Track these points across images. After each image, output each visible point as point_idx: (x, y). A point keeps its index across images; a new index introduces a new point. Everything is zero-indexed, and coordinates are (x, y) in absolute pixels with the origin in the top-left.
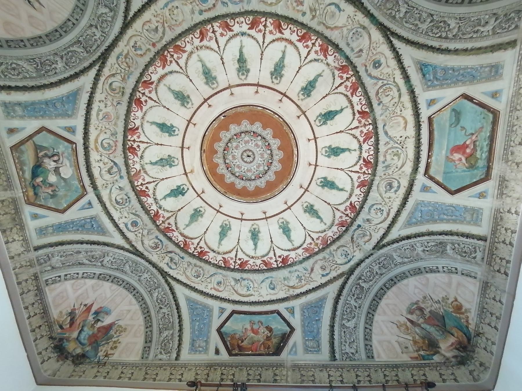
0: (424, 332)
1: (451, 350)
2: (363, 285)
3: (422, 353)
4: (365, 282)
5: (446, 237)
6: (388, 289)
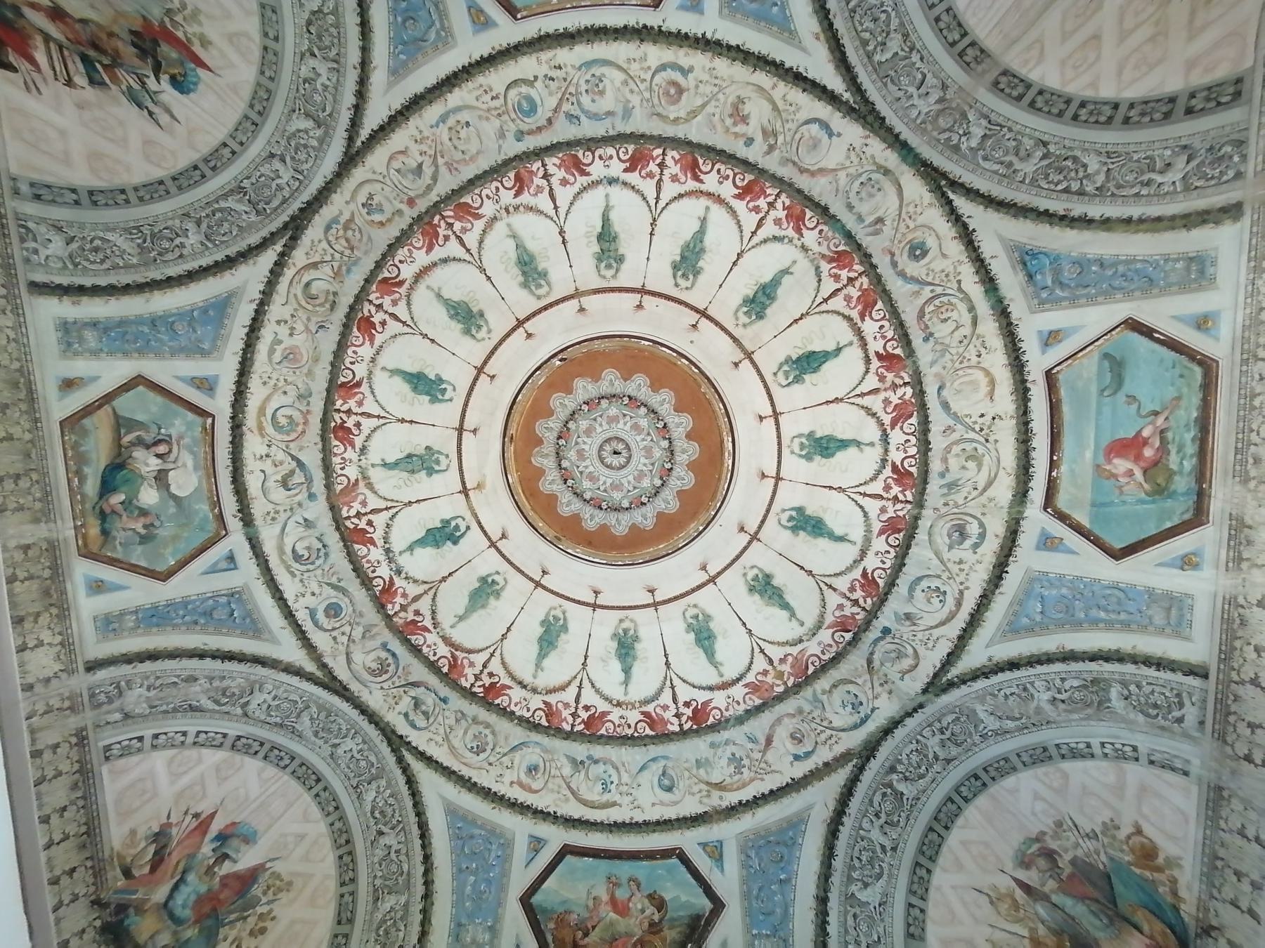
2: (901, 787)
4: (906, 779)
6: (966, 800)
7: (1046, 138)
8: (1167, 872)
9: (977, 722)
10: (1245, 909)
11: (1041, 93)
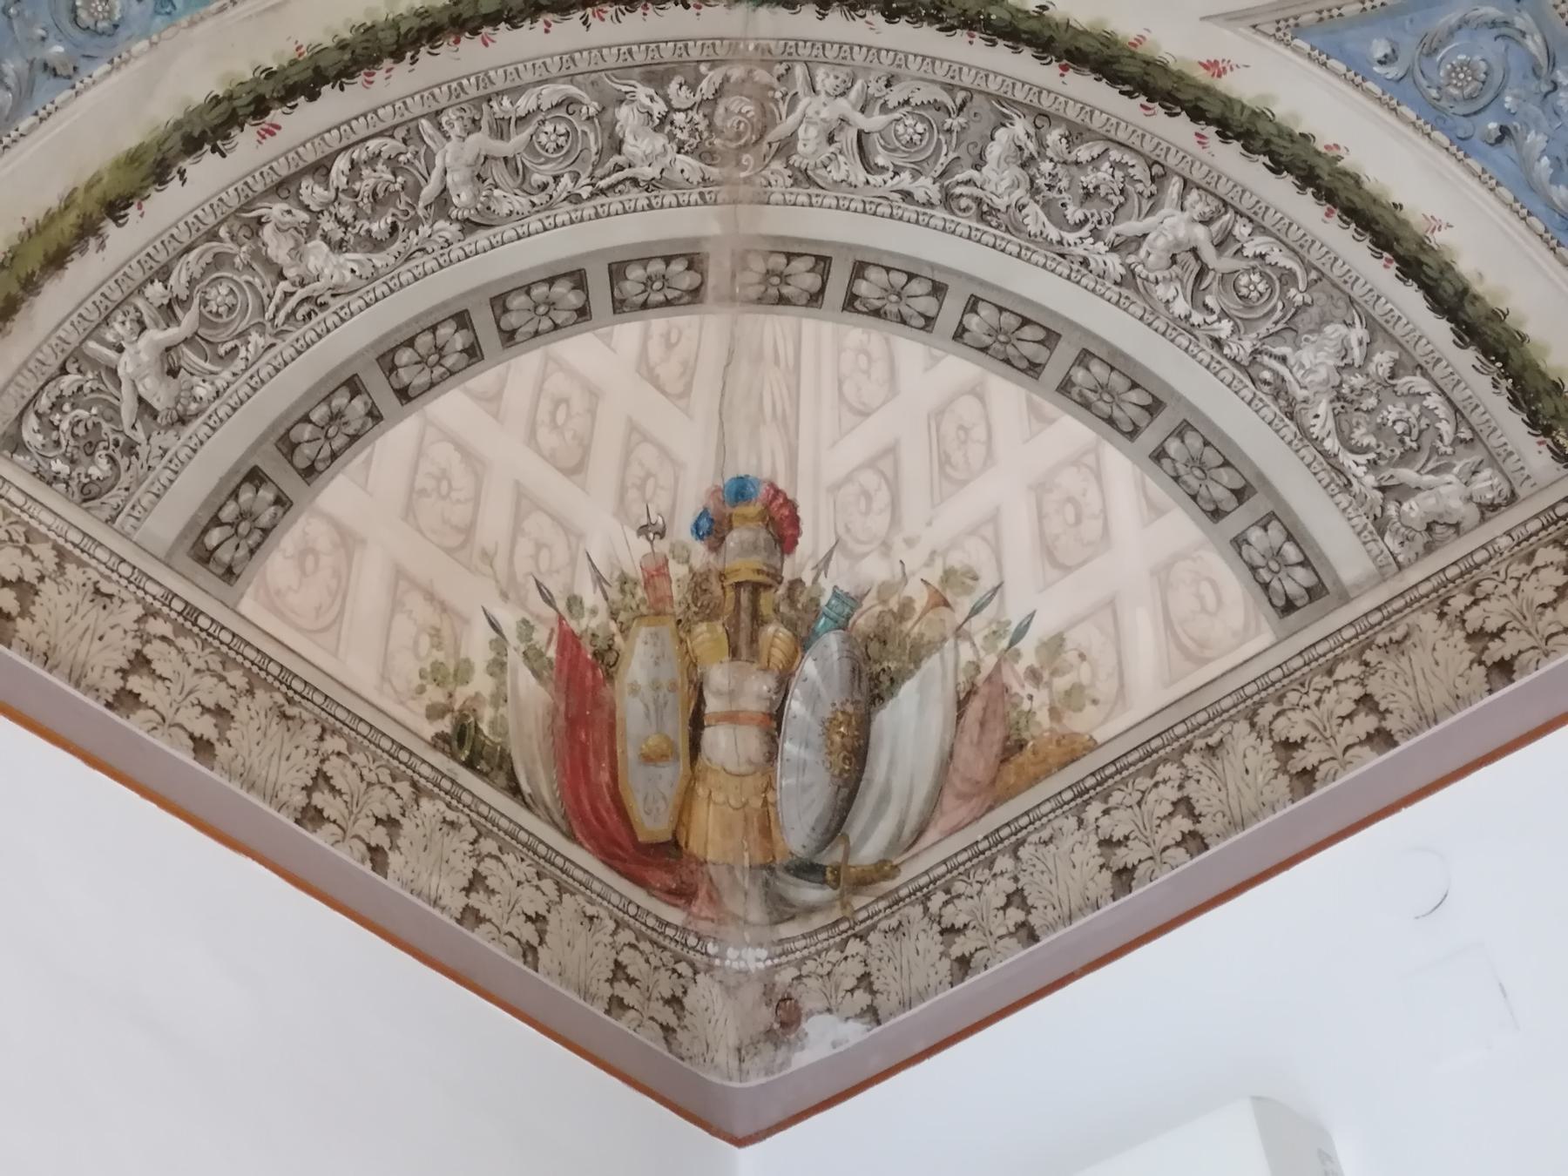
7: (481, 238)
11: (583, 313)
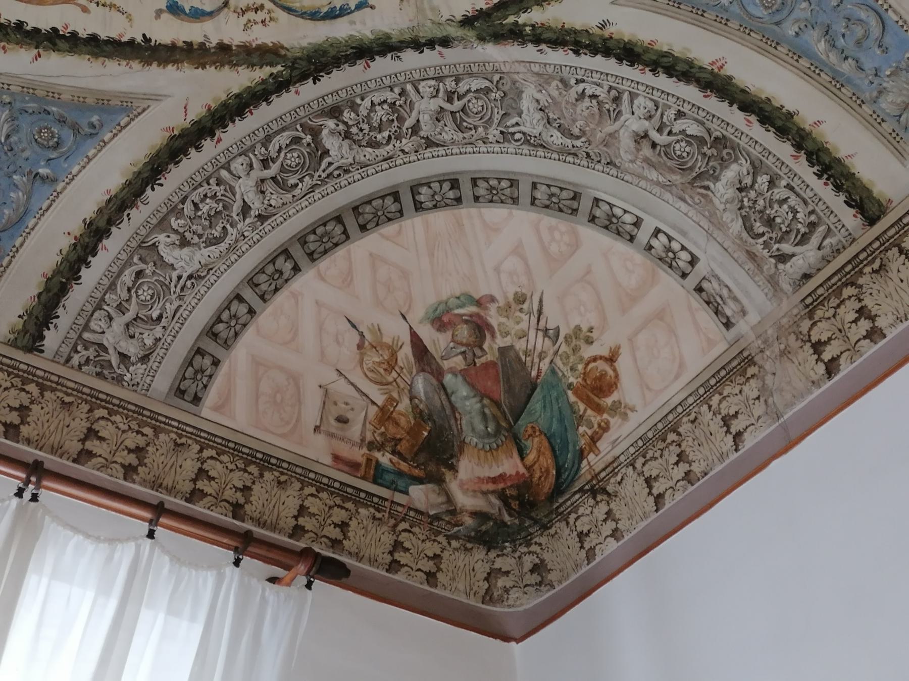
0: (438, 400)
1: (485, 493)
2: (330, 142)
3: (385, 459)
4: (347, 135)
5: (757, 131)
6: (419, 207)
8: (605, 416)
9: (511, 107)
10: (655, 492)
